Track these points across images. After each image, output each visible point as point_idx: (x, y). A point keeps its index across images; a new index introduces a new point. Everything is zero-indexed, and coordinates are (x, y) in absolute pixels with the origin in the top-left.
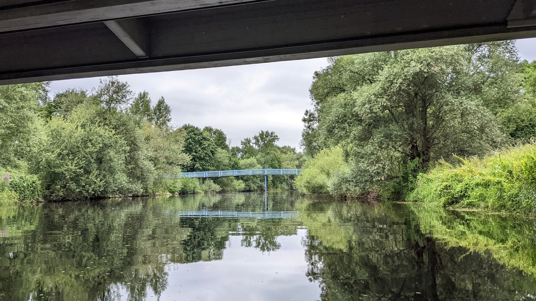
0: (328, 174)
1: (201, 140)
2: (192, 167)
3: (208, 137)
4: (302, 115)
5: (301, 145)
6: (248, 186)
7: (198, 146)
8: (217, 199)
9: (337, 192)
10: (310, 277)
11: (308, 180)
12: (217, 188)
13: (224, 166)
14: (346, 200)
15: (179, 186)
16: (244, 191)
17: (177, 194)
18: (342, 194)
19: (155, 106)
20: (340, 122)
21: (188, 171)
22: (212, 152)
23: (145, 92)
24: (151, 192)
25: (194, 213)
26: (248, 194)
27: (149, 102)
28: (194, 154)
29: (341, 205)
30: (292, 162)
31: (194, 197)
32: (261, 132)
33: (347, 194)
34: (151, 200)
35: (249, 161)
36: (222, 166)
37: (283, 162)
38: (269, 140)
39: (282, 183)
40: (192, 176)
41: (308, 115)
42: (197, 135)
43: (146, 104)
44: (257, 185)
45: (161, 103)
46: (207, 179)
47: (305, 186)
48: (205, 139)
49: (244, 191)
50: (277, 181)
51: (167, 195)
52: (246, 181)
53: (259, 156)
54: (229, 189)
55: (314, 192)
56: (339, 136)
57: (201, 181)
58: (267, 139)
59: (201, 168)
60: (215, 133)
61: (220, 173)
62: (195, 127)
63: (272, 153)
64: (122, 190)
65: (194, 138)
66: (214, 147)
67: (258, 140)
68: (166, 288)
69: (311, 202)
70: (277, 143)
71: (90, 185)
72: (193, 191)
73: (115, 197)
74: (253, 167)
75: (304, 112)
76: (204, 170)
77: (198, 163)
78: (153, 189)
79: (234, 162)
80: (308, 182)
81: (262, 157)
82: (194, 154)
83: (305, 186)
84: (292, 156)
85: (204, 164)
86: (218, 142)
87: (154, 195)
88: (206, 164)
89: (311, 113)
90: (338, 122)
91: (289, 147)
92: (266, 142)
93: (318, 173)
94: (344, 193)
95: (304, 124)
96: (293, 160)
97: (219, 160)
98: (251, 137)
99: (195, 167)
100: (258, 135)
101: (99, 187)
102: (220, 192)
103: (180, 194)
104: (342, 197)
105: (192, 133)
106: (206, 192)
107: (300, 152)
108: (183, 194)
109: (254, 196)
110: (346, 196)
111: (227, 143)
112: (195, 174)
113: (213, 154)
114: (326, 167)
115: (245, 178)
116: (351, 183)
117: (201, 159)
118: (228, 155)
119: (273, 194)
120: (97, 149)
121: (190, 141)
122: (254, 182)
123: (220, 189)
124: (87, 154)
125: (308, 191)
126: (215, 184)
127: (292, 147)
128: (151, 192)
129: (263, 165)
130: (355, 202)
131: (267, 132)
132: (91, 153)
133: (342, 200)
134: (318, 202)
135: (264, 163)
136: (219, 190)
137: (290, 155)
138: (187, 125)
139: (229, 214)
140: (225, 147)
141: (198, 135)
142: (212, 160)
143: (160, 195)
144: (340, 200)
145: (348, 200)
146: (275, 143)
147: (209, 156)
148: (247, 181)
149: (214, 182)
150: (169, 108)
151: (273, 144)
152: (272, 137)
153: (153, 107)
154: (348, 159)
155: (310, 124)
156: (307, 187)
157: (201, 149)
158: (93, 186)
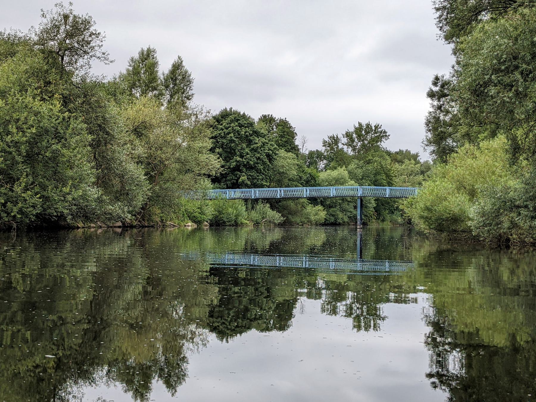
0: (472, 194)
1: (251, 136)
2: (235, 181)
3: (262, 131)
4: (428, 85)
5: (427, 145)
6: (333, 216)
7: (244, 145)
8: (277, 235)
9: (489, 231)
10: (433, 380)
11: (428, 204)
12: (276, 216)
13: (289, 180)
14: (508, 247)
15: (210, 212)
16: (325, 224)
17: (206, 225)
18: (500, 235)
19: (167, 72)
20: (502, 71)
21: (228, 188)
22: (268, 156)
23: (149, 48)
24: (158, 219)
25: (238, 259)
26: (330, 229)
27: (154, 65)
28: (238, 159)
29: (498, 257)
30: (411, 177)
31: (236, 232)
32: (357, 126)
33: (511, 235)
34: (158, 233)
35: (335, 174)
36: (286, 181)
37: (396, 176)
38: (371, 139)
39: (393, 213)
40: (233, 196)
41: (439, 84)
42: (243, 126)
43: (152, 68)
44: (349, 214)
45: (177, 67)
46: (260, 202)
47: (421, 217)
48: (257, 133)
49: (325, 224)
50: (385, 209)
51: (188, 226)
52: (330, 207)
53: (352, 166)
54: (298, 220)
55: (440, 228)
56: (499, 102)
57: (250, 206)
58: (369, 137)
59: (249, 183)
60: (278, 125)
61: (279, 193)
62: (240, 112)
63: (376, 161)
64: (94, 214)
65: (238, 131)
66: (272, 148)
67: (352, 138)
68: (185, 380)
69: (434, 249)
70: (385, 145)
71: (15, 203)
72: (235, 221)
73: (89, 227)
74: (342, 184)
75: (432, 78)
76: (255, 186)
77: (244, 174)
78: (162, 215)
79: (308, 175)
80: (428, 209)
81: (359, 167)
82: (238, 159)
83: (421, 217)
84: (412, 167)
85: (255, 175)
86: (281, 140)
87: (164, 226)
88: (258, 176)
89: (446, 82)
90: (496, 71)
91: (408, 152)
92: (366, 142)
93: (451, 191)
94: (505, 233)
95: (431, 102)
96: (414, 175)
97: (281, 170)
98: (340, 133)
99: (240, 180)
100: (352, 130)
101: (32, 206)
102: (281, 225)
103: (211, 225)
104: (499, 241)
105: (234, 124)
106: (257, 224)
107: (427, 162)
108: (216, 226)
109: (342, 232)
110: (508, 240)
111: (298, 142)
112: (237, 193)
113: (270, 160)
114: (469, 180)
115: (328, 203)
116: (523, 212)
117: (250, 168)
118: (296, 162)
119: (377, 230)
120: (26, 137)
121: (231, 137)
122: (343, 210)
123: (282, 218)
124: (9, 147)
125: (428, 228)
126: (273, 210)
127: (413, 152)
128: (158, 219)
129: (360, 181)
130: (528, 252)
131: (368, 125)
132: (16, 144)
133: (499, 246)
134: (448, 250)
135: (361, 177)
136: (279, 221)
137: (409, 165)
138: (228, 110)
139: (303, 262)
140: (294, 149)
141: (246, 127)
142: (268, 170)
143: (174, 226)
144: (495, 246)
145: (512, 247)
146: (382, 143)
147: (264, 163)
148: (330, 207)
149: (272, 208)
150: (190, 76)
151: (378, 146)
152: (376, 133)
153: (164, 74)
154: (518, 159)
155: (441, 103)
156: (426, 219)
157: (251, 151)
158: (20, 205)
